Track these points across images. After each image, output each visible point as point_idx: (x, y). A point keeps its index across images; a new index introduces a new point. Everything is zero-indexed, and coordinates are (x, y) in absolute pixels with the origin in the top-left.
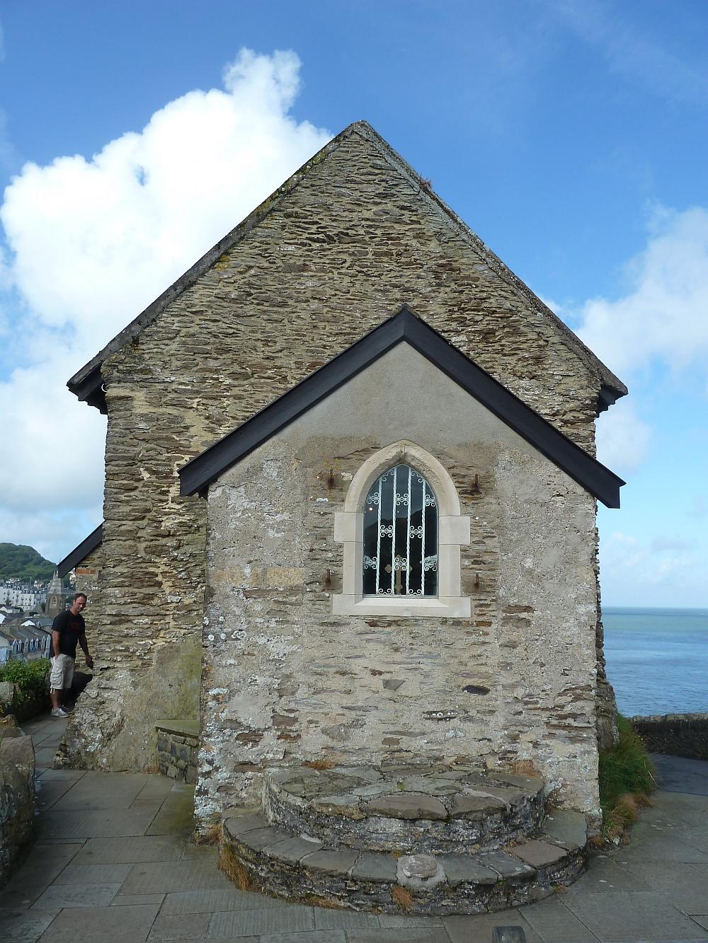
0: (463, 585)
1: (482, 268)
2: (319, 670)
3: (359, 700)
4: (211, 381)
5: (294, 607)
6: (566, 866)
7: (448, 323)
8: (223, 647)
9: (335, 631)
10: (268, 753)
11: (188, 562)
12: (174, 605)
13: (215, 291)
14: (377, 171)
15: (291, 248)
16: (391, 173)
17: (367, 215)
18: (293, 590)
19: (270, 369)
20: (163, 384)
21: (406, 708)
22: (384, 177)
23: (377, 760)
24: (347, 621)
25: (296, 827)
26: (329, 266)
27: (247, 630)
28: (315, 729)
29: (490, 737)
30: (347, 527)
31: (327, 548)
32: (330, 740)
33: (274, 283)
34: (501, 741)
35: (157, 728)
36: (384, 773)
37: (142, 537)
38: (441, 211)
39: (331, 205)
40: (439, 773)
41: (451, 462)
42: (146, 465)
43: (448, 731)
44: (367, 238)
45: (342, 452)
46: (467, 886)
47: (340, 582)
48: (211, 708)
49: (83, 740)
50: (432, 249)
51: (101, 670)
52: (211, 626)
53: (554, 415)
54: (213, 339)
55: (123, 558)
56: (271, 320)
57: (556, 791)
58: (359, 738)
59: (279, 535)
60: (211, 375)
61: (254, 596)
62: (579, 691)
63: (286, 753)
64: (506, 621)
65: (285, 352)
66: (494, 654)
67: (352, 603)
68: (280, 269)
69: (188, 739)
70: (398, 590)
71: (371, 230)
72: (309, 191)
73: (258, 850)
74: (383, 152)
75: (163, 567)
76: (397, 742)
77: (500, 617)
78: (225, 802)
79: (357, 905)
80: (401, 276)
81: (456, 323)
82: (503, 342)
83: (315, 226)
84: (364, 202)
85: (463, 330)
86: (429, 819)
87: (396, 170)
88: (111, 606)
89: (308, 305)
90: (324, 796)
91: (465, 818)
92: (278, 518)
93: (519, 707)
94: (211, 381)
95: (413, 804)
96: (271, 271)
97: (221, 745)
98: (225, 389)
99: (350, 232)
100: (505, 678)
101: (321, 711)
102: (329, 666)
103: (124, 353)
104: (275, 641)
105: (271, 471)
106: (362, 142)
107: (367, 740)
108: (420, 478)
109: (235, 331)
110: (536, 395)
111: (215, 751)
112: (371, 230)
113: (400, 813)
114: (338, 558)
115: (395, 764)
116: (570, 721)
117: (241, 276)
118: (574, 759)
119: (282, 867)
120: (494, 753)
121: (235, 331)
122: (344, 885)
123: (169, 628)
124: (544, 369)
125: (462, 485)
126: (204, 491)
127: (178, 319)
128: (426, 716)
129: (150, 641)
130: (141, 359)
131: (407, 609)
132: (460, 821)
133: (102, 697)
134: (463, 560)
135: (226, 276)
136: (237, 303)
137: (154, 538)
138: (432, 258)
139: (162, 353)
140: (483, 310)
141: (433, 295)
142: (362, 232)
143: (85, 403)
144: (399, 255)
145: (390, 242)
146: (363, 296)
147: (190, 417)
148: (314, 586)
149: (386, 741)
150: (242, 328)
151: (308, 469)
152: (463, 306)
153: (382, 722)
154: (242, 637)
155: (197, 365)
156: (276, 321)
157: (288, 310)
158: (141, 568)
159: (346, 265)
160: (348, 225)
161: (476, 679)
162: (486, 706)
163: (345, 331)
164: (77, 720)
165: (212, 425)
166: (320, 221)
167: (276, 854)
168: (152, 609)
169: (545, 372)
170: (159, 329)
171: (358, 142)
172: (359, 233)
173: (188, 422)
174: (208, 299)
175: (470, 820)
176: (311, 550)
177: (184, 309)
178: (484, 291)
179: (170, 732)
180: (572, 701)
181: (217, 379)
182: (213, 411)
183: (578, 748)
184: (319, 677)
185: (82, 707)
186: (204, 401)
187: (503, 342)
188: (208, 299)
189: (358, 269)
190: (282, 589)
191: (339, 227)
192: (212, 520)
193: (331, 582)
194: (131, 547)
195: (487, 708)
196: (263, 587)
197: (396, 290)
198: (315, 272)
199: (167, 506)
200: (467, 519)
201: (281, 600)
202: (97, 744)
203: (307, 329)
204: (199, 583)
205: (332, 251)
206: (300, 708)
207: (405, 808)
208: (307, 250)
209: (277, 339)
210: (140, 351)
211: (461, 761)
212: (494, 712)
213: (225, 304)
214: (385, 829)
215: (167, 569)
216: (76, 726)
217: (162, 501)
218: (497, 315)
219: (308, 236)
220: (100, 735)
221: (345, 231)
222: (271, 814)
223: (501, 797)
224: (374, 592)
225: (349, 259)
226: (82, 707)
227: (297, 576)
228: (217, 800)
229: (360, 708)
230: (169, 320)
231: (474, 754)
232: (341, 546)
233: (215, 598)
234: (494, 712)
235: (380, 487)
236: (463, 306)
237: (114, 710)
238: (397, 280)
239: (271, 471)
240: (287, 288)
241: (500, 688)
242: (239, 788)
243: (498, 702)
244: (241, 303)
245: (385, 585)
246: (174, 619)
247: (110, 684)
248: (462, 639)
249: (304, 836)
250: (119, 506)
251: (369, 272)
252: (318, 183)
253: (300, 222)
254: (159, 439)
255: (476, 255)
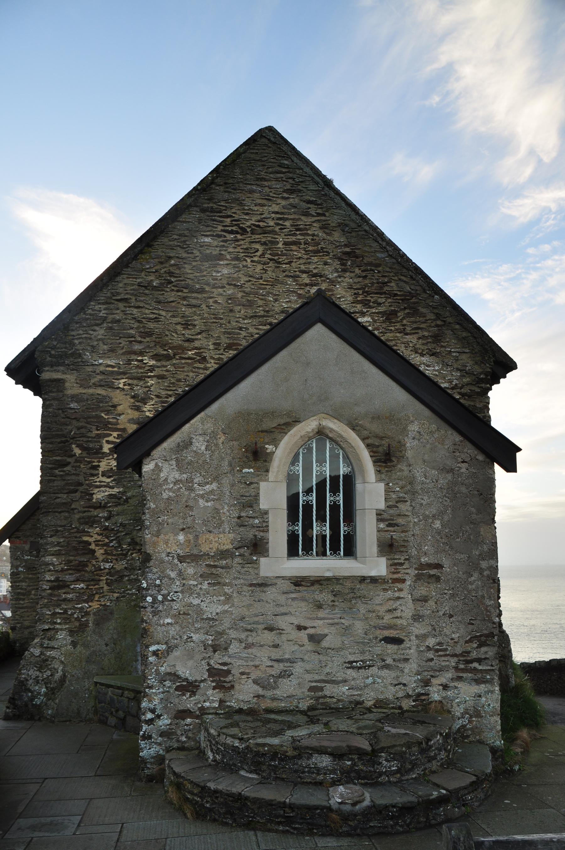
0: (379, 546)
1: (383, 255)
2: (249, 627)
3: (286, 653)
4: (136, 363)
5: (224, 570)
6: (476, 790)
7: (354, 305)
8: (160, 608)
9: (263, 592)
10: (204, 702)
11: (118, 531)
12: (107, 571)
13: (138, 280)
14: (284, 170)
15: (208, 240)
16: (298, 171)
17: (276, 208)
18: (223, 554)
19: (190, 350)
20: (91, 367)
21: (329, 659)
22: (291, 175)
23: (304, 705)
24: (275, 581)
25: (235, 765)
26: (243, 255)
27: (182, 592)
28: (246, 680)
29: (405, 682)
30: (272, 496)
31: (254, 515)
32: (260, 689)
33: (192, 272)
34: (415, 685)
35: (96, 683)
36: (311, 715)
37: (76, 509)
38: (343, 204)
39: (244, 200)
40: (361, 715)
41: (365, 433)
42: (78, 442)
43: (368, 678)
44: (277, 229)
45: (265, 427)
46: (391, 809)
47: (267, 546)
48: (151, 663)
49: (30, 694)
50: (337, 239)
51: (42, 631)
52: (149, 589)
53: (453, 388)
54: (136, 325)
55: (59, 529)
56: (190, 305)
57: (463, 726)
58: (287, 688)
59: (209, 504)
60: (135, 357)
61: (187, 561)
62: (483, 639)
63: (221, 701)
64: (418, 577)
65: (204, 335)
66: (407, 609)
67: (278, 563)
68: (198, 259)
69: (126, 692)
70: (320, 553)
71: (281, 222)
72: (222, 189)
73: (202, 784)
74: (289, 153)
75: (96, 536)
76: (321, 689)
77: (413, 574)
78: (167, 745)
79: (295, 829)
80: (309, 263)
81: (361, 305)
82: (405, 322)
83: (229, 220)
84: (273, 197)
85: (367, 311)
86: (356, 754)
87: (302, 169)
88: (49, 573)
89: (224, 291)
90: (260, 737)
91: (387, 752)
92: (208, 488)
93: (430, 655)
94: (136, 363)
95: (339, 741)
96: (190, 261)
97: (161, 696)
98: (149, 370)
99: (261, 224)
100: (418, 629)
101: (252, 663)
102: (257, 623)
103: (56, 339)
104: (208, 601)
105: (200, 445)
106: (270, 145)
107: (294, 689)
108: (337, 448)
109: (157, 316)
110: (436, 371)
111: (156, 702)
112: (281, 222)
113: (329, 750)
114: (264, 525)
115: (319, 711)
116: (475, 665)
117: (162, 266)
118: (478, 698)
119: (226, 799)
120: (408, 696)
121: (157, 316)
122: (282, 812)
123: (103, 593)
124: (442, 346)
125: (376, 454)
126: (137, 467)
127: (105, 306)
128: (348, 665)
129: (86, 605)
130: (72, 344)
131: (328, 570)
132: (383, 754)
133: (44, 655)
134: (379, 523)
135: (148, 266)
136: (159, 290)
137: (86, 509)
138: (338, 247)
139: (90, 339)
140: (385, 293)
141: (339, 280)
142: (271, 223)
143: (20, 386)
144: (307, 244)
145: (298, 233)
146: (275, 282)
147: (117, 397)
148: (242, 551)
149: (311, 689)
150: (163, 313)
151: (234, 442)
152: (367, 289)
153: (308, 672)
154: (178, 598)
155: (123, 348)
156: (195, 306)
157: (205, 295)
158: (76, 537)
159: (258, 254)
160: (259, 217)
161: (392, 631)
162: (400, 654)
163: (259, 314)
164: (23, 676)
165: (137, 404)
166: (234, 215)
167: (220, 787)
168: (87, 575)
169: (443, 349)
170: (87, 317)
171: (266, 145)
172: (270, 225)
173: (115, 401)
174: (132, 288)
175: (392, 753)
176: (239, 517)
177: (111, 298)
178: (385, 276)
179: (108, 686)
180: (477, 648)
181: (142, 361)
182: (139, 391)
183: (483, 688)
184: (249, 633)
185: (27, 665)
186: (130, 382)
187: (405, 322)
188: (132, 288)
189: (270, 257)
190: (213, 554)
191: (251, 220)
192: (147, 492)
193: (258, 547)
194: (66, 518)
195: (402, 657)
196: (195, 552)
197: (304, 275)
198: (230, 260)
199: (98, 480)
200: (382, 486)
201: (212, 563)
202: (42, 698)
203: (223, 313)
204: (129, 550)
205: (245, 241)
206: (232, 662)
207: (334, 745)
208: (223, 241)
209: (196, 323)
210: (71, 337)
211: (380, 704)
212: (408, 659)
213: (147, 292)
214: (316, 764)
215: (99, 538)
216: (22, 682)
217: (93, 475)
218: (399, 298)
219: (223, 228)
220: (44, 690)
221: (257, 223)
222: (210, 755)
223: (417, 733)
224: (297, 555)
225: (261, 248)
226: (27, 665)
227: (225, 540)
228: (160, 744)
229: (288, 660)
230: (97, 307)
231: (391, 697)
232: (266, 513)
233: (151, 563)
234: (408, 659)
235: (301, 458)
236: (367, 289)
237: (56, 667)
238: (306, 267)
239: (200, 445)
240: (204, 276)
241: (413, 638)
242: (179, 733)
243: (412, 651)
244: (163, 290)
245: (307, 549)
246: (107, 584)
247: (52, 644)
248: (378, 595)
249: (242, 773)
250: (54, 480)
251: (280, 260)
252: (230, 181)
253: (215, 216)
254: (89, 418)
255: (376, 244)
